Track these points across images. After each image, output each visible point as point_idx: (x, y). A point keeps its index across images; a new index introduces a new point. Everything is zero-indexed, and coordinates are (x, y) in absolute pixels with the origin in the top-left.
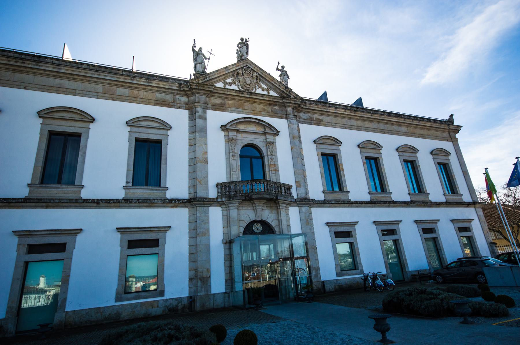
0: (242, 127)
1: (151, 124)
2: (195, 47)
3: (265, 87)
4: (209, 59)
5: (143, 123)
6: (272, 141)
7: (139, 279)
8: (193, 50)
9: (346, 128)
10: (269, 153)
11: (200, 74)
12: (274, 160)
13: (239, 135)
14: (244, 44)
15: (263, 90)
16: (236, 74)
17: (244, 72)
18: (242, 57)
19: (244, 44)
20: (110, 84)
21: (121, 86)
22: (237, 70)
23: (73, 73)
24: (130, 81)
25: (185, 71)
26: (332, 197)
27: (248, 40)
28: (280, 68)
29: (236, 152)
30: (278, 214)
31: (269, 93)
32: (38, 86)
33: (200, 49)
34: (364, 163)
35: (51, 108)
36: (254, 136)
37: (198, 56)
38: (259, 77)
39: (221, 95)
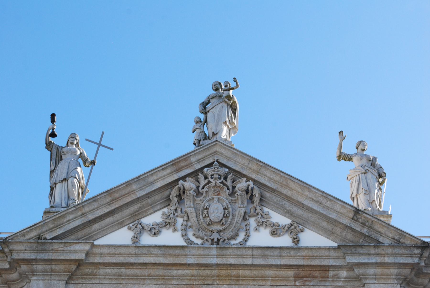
2: (53, 135)
3: (284, 221)
4: (93, 163)
8: (49, 145)
15: (276, 231)
16: (174, 192)
17: (203, 182)
19: (222, 96)
22: (177, 181)
28: (349, 148)
31: (296, 241)
38: (257, 192)
39: (116, 270)
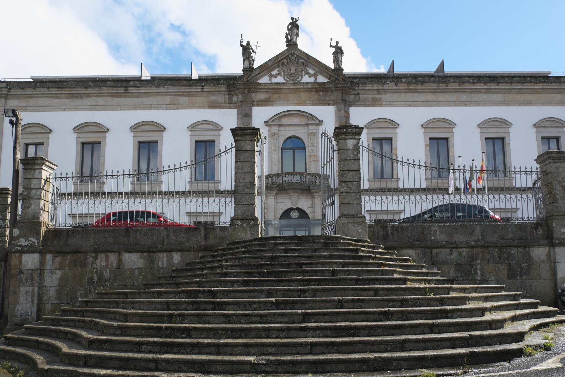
0: (285, 121)
1: (206, 127)
5: (200, 127)
6: (315, 131)
7: (557, 239)
8: (241, 45)
9: (409, 106)
10: (310, 144)
11: (249, 70)
12: (315, 151)
13: (282, 128)
14: (294, 26)
16: (281, 64)
18: (291, 44)
19: (294, 26)
20: (175, 95)
21: (182, 95)
23: (148, 91)
24: (189, 90)
25: (235, 67)
26: (378, 185)
27: (297, 19)
29: (277, 145)
30: (313, 202)
32: (128, 106)
33: (248, 43)
34: (426, 145)
35: (137, 124)
36: (296, 128)
37: (247, 50)
